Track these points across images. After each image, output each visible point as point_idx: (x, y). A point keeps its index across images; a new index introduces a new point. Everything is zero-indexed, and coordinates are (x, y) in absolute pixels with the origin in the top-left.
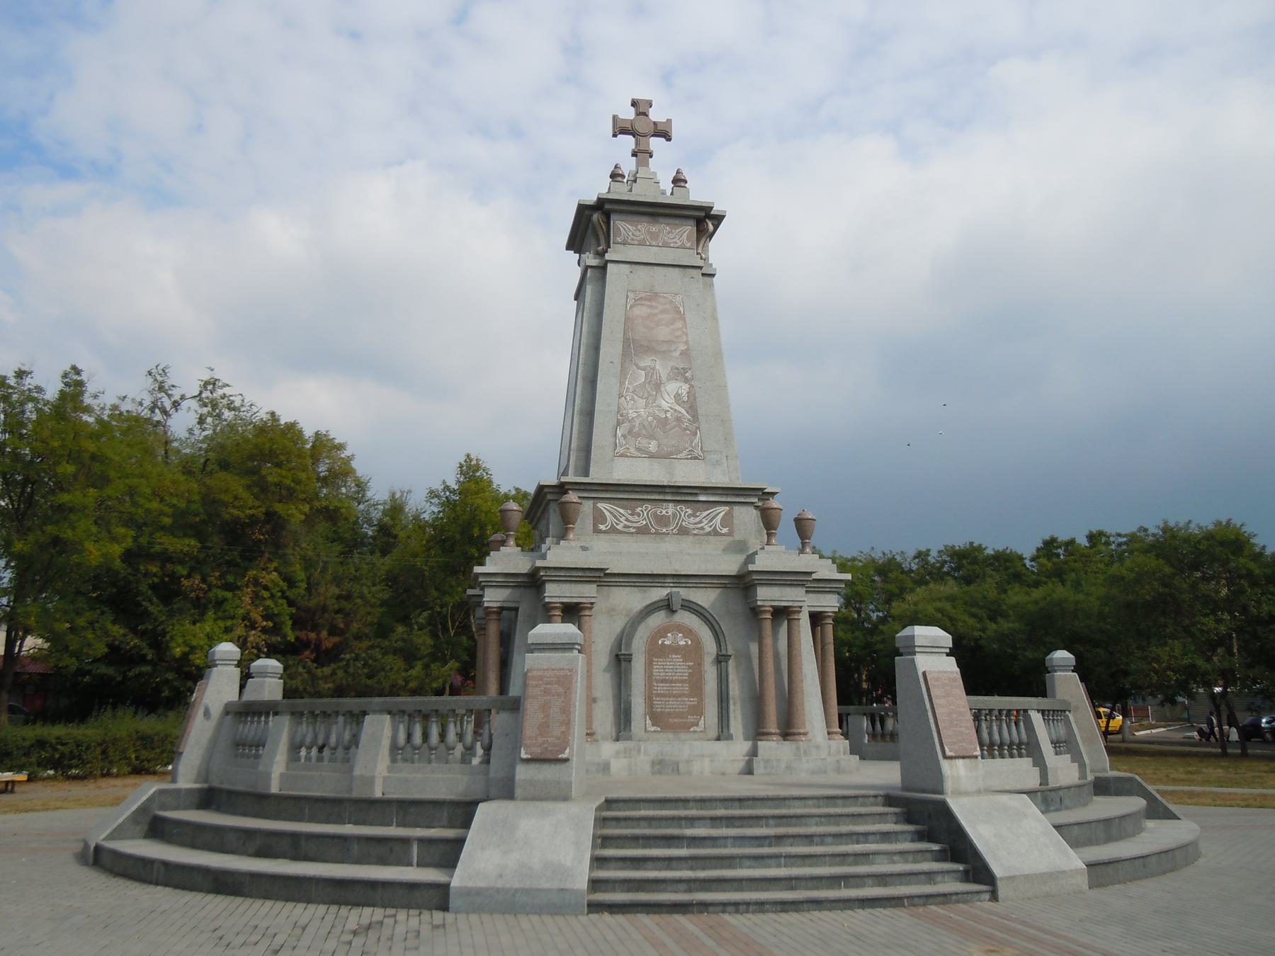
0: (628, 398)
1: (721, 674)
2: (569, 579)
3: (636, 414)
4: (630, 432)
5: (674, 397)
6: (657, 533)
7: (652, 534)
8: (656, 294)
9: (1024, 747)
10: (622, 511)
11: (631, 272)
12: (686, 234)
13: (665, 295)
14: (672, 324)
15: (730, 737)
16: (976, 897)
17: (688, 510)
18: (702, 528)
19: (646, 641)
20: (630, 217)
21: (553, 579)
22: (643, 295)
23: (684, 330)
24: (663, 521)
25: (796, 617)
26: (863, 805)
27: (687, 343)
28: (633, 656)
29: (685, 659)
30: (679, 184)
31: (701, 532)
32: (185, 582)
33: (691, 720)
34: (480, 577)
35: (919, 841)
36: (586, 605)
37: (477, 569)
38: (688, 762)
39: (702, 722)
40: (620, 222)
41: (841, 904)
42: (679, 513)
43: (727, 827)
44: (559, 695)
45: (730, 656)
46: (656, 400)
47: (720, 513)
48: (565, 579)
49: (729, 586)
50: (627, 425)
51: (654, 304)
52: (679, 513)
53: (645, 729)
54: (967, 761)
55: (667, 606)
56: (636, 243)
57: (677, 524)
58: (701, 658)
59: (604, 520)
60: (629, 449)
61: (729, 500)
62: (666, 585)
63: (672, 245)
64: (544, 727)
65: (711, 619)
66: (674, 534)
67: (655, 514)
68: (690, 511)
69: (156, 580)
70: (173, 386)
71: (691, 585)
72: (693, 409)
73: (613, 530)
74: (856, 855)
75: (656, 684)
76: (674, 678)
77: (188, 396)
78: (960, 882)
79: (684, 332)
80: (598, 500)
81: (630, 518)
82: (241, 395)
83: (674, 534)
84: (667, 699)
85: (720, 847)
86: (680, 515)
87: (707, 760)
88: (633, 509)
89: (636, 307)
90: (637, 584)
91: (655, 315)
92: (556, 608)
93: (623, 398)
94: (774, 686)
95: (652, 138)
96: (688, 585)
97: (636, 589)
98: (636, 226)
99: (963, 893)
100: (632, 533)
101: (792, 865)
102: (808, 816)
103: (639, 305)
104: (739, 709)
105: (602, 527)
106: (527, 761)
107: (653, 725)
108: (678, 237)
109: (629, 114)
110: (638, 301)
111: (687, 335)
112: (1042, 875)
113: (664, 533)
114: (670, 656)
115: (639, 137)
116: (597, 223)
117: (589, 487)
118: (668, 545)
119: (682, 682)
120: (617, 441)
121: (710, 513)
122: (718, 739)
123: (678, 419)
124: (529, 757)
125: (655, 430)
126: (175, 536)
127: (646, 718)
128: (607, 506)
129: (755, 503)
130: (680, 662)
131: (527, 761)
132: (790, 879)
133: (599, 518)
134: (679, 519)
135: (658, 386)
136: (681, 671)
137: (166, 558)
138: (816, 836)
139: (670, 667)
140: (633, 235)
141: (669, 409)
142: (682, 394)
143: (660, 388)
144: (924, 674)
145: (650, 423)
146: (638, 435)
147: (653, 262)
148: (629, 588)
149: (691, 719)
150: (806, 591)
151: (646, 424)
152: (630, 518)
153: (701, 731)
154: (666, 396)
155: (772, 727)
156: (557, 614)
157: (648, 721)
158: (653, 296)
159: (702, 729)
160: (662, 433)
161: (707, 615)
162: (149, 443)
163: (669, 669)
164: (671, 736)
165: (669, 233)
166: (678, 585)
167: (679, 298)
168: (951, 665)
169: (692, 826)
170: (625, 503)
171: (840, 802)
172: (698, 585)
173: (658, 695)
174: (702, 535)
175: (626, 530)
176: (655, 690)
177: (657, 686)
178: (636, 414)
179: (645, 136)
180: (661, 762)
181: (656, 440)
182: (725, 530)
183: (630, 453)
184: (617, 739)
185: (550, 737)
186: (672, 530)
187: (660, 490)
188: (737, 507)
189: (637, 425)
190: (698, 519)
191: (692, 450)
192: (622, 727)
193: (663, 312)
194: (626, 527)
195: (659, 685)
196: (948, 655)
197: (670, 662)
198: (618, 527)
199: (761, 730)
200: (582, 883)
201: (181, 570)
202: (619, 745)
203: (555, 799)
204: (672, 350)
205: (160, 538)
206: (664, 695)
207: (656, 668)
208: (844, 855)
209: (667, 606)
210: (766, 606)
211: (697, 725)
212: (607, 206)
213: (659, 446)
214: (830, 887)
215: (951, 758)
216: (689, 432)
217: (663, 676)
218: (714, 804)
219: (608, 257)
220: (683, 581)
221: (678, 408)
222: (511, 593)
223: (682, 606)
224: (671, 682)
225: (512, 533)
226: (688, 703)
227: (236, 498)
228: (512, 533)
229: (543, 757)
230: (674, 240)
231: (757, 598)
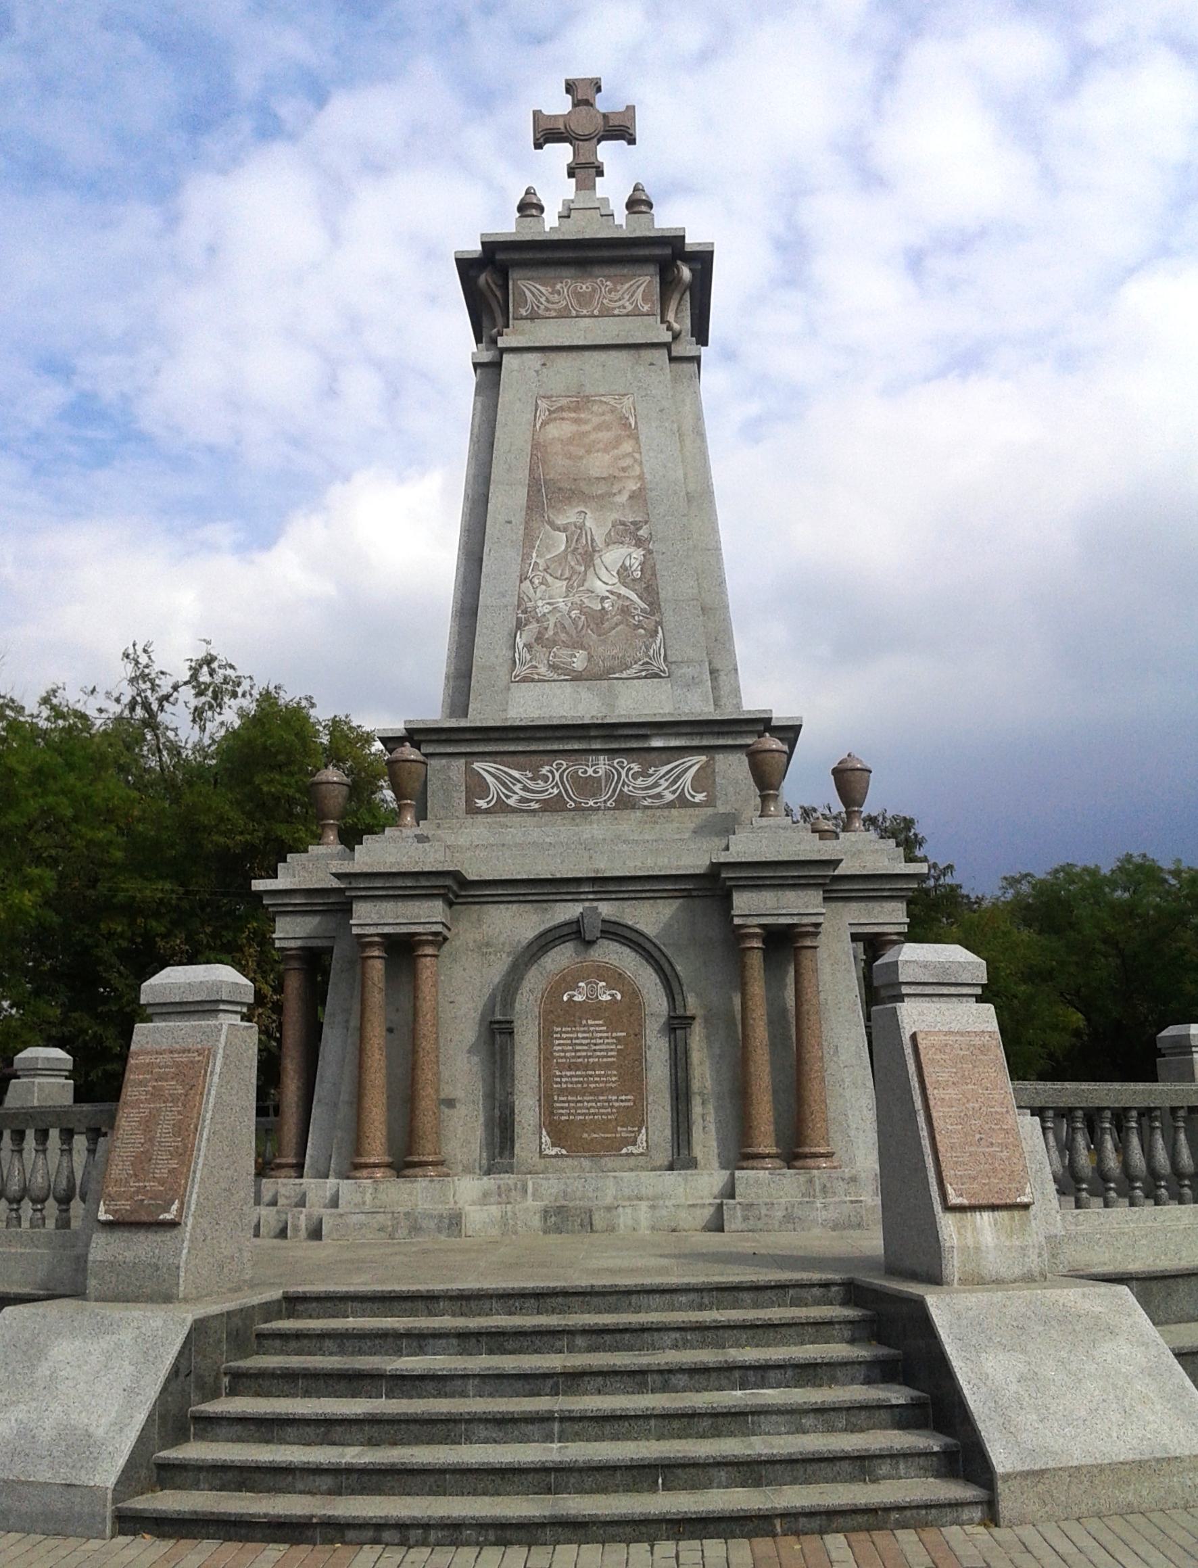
0: (536, 581)
1: (676, 1050)
2: (391, 893)
3: (550, 608)
4: (539, 639)
5: (618, 573)
6: (578, 808)
7: (570, 810)
8: (587, 399)
9: (1187, 1182)
10: (515, 773)
11: (544, 365)
12: (642, 288)
13: (603, 399)
14: (615, 447)
15: (691, 1164)
16: (950, 1515)
17: (632, 765)
18: (659, 796)
19: (540, 996)
20: (541, 272)
21: (363, 893)
22: (564, 402)
23: (637, 456)
24: (588, 786)
25: (809, 943)
26: (797, 1303)
27: (641, 477)
28: (515, 1024)
29: (612, 1026)
30: (636, 209)
31: (658, 802)
32: (160, 943)
33: (624, 1135)
34: (264, 898)
35: (882, 1383)
36: (424, 938)
37: (258, 885)
38: (609, 1209)
39: (642, 1136)
40: (523, 282)
41: (628, 1530)
42: (617, 770)
43: (491, 1352)
44: (175, 1099)
45: (693, 1018)
46: (584, 580)
47: (690, 767)
48: (384, 893)
49: (694, 893)
50: (533, 627)
51: (582, 416)
52: (617, 770)
53: (541, 1152)
54: (999, 1215)
55: (575, 933)
56: (554, 314)
57: (614, 790)
58: (641, 1025)
59: (484, 790)
60: (536, 667)
61: (705, 743)
62: (583, 897)
63: (616, 312)
64: (142, 1162)
65: (656, 954)
66: (609, 809)
67: (575, 777)
68: (636, 767)
69: (124, 944)
70: (162, 673)
71: (626, 896)
72: (650, 592)
73: (501, 808)
74: (715, 1415)
75: (558, 1073)
76: (591, 1060)
77: (181, 683)
78: (936, 1477)
79: (636, 461)
80: (474, 758)
81: (531, 785)
82: (251, 678)
83: (609, 809)
84: (579, 1098)
85: (452, 1396)
86: (619, 774)
87: (644, 1205)
88: (535, 770)
89: (551, 425)
90: (530, 898)
91: (585, 434)
92: (371, 944)
93: (528, 581)
94: (768, 1069)
95: (603, 143)
96: (621, 896)
97: (529, 906)
98: (553, 286)
99: (918, 1507)
100: (534, 811)
101: (577, 1437)
102: (658, 1330)
103: (555, 419)
104: (712, 1111)
105: (482, 803)
106: (109, 1225)
107: (554, 1145)
108: (627, 297)
109: (559, 105)
110: (555, 414)
111: (641, 464)
112: (1114, 1467)
113: (591, 808)
114: (584, 1022)
115: (577, 142)
116: (486, 286)
117: (454, 736)
118: (597, 829)
119: (608, 1066)
120: (517, 655)
121: (672, 769)
122: (671, 1168)
123: (625, 611)
124: (111, 1218)
125: (584, 631)
126: (146, 879)
127: (541, 1133)
128: (489, 766)
129: (749, 746)
130: (601, 1032)
131: (109, 1225)
132: (544, 1470)
133: (477, 787)
134: (617, 783)
135: (589, 557)
136: (604, 1047)
137: (131, 910)
138: (652, 1372)
139: (584, 1042)
140: (548, 301)
141: (607, 594)
142: (631, 567)
143: (592, 560)
144: (914, 1037)
145: (574, 622)
146: (550, 644)
147: (580, 343)
148: (515, 906)
149: (622, 1132)
150: (825, 898)
151: (568, 622)
152: (531, 785)
153: (642, 1154)
154: (603, 573)
155: (766, 1143)
156: (376, 953)
157: (546, 1139)
158: (581, 402)
159: (641, 1150)
160: (594, 636)
161: (648, 946)
162: (94, 747)
163: (581, 1044)
164: (586, 1163)
165: (610, 292)
166: (603, 896)
167: (627, 402)
168: (985, 1018)
169: (421, 1351)
170: (522, 759)
171: (746, 1296)
172: (639, 895)
173: (562, 1091)
174: (658, 807)
175: (524, 806)
176: (557, 1083)
177: (561, 1077)
178: (550, 608)
179: (587, 139)
180: (560, 1211)
181: (585, 649)
182: (700, 797)
183: (538, 674)
184: (488, 1172)
185: (149, 1181)
186: (605, 802)
187: (579, 733)
188: (721, 755)
189: (551, 626)
190: (651, 781)
191: (647, 663)
192: (497, 1151)
193: (598, 428)
194: (523, 800)
195: (564, 1073)
196: (980, 999)
197: (584, 1032)
198: (510, 802)
199: (750, 1150)
200: (107, 1475)
201: (157, 926)
202: (488, 1182)
203: (151, 1299)
204: (614, 491)
205: (124, 882)
206: (573, 1092)
207: (559, 1045)
208: (692, 1416)
209: (575, 933)
210: (749, 927)
211: (634, 1143)
212: (500, 256)
213: (590, 658)
214: (631, 1488)
215: (961, 1209)
216: (642, 631)
217: (573, 1057)
218: (487, 1306)
219: (502, 342)
220: (611, 889)
221: (624, 591)
222: (319, 923)
223: (602, 931)
224: (587, 1067)
225: (332, 822)
226: (616, 1104)
227: (221, 819)
228: (332, 822)
229: (133, 1218)
230: (621, 303)
231: (733, 913)
